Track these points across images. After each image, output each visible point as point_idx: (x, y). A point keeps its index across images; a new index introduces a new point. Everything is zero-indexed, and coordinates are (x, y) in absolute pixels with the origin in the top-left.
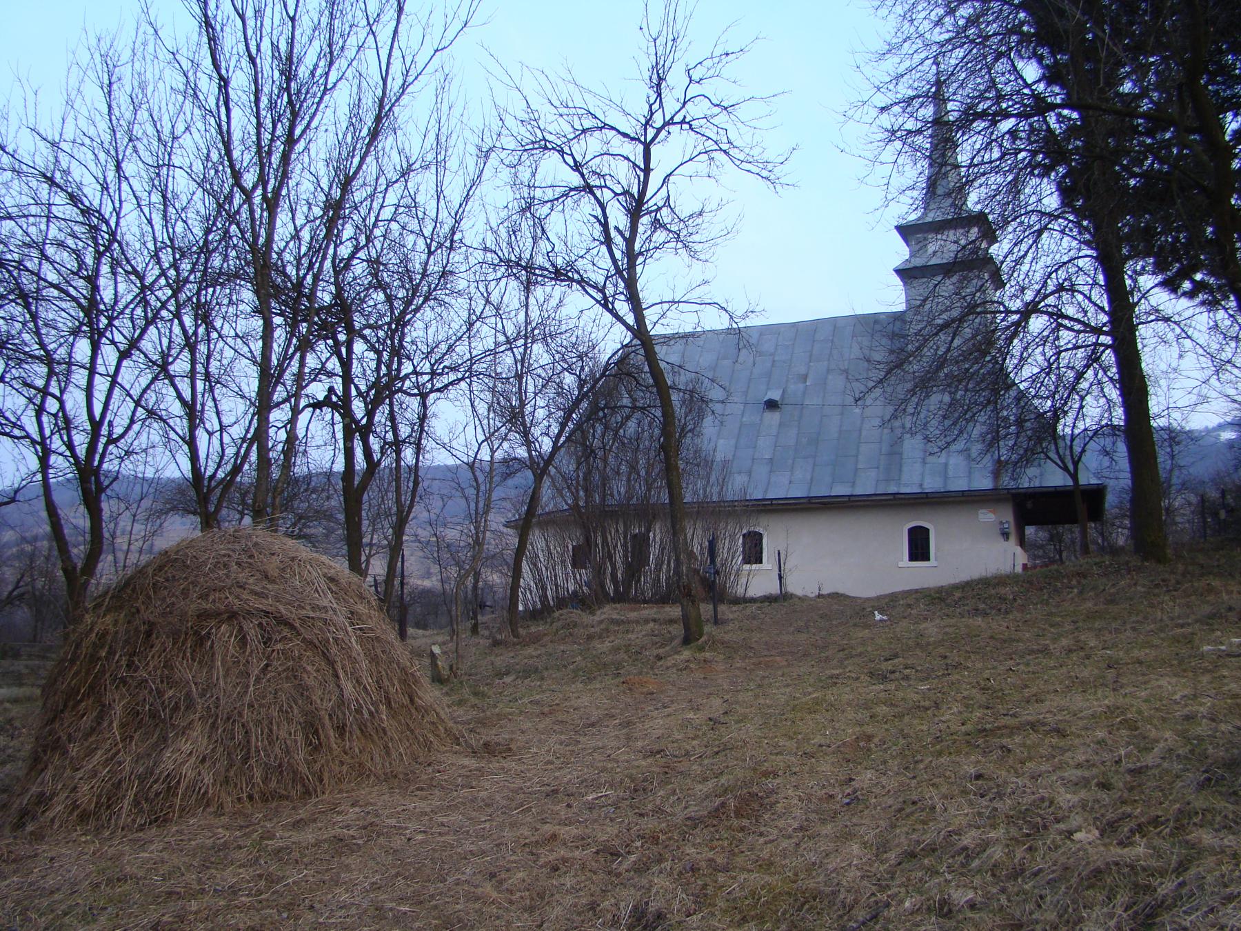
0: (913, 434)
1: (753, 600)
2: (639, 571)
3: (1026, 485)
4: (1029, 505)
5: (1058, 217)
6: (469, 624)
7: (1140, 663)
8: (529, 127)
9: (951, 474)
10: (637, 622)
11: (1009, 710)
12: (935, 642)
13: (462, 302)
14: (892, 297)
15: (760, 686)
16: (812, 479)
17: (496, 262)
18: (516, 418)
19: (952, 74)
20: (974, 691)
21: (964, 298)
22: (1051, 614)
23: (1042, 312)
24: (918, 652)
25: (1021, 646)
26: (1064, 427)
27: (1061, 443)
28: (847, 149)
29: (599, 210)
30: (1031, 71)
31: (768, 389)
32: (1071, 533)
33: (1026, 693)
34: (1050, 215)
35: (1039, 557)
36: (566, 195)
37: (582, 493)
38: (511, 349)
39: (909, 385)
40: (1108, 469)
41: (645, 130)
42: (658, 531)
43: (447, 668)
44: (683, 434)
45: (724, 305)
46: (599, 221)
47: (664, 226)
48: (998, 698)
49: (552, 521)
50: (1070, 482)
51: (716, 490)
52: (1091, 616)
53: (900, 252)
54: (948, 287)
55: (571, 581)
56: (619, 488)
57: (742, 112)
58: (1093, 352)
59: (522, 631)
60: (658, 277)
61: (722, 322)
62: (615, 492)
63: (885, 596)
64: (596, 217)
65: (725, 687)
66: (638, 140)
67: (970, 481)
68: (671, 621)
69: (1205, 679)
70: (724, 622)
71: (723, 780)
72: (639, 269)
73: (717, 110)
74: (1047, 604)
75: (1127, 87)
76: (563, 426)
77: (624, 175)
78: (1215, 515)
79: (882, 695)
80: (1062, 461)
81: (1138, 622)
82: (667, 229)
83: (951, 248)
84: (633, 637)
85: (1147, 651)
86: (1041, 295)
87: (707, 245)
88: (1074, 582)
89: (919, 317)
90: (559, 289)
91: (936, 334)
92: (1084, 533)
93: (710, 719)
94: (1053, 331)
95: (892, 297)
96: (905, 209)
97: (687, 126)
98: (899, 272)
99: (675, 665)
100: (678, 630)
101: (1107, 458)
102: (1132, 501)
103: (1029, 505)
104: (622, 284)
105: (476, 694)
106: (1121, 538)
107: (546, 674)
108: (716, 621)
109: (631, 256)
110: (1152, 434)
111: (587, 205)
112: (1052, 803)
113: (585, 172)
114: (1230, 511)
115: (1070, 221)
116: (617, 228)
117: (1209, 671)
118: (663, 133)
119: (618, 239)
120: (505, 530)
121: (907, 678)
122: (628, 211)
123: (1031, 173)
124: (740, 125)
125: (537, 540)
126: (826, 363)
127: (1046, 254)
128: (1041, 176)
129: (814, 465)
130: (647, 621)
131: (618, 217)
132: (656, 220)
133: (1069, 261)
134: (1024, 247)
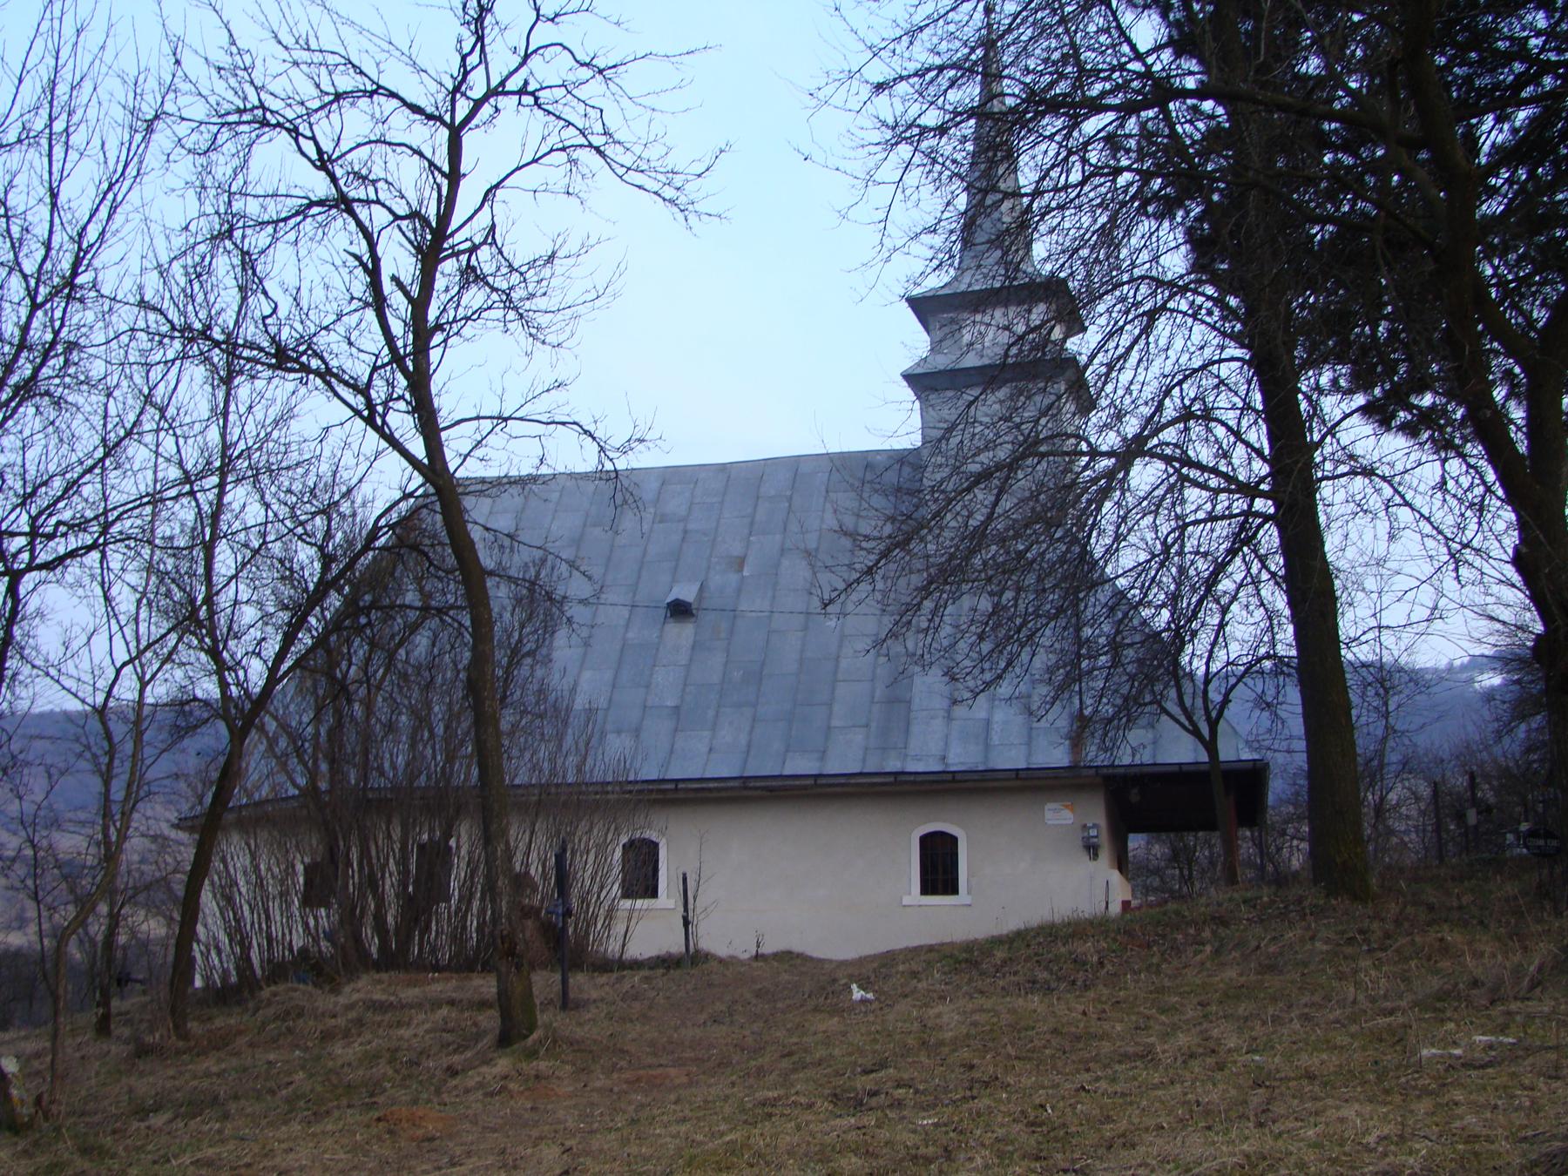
0: (926, 667)
1: (636, 965)
3: (1127, 760)
4: (1134, 795)
5: (1184, 290)
6: (91, 1016)
7: (1311, 1077)
8: (233, 81)
9: (995, 739)
10: (419, 1006)
11: (1074, 1161)
12: (954, 1041)
13: (88, 402)
14: (897, 424)
15: (634, 1122)
16: (749, 746)
17: (165, 329)
18: (197, 620)
19: (1009, 30)
20: (1017, 1127)
21: (1018, 426)
22: (1161, 990)
23: (1153, 456)
25: (1106, 1047)
26: (1194, 658)
27: (1187, 687)
28: (818, 155)
29: (364, 243)
30: (1146, 30)
31: (674, 581)
32: (1205, 846)
33: (1108, 1131)
34: (1171, 284)
35: (1155, 890)
36: (302, 212)
37: (324, 767)
38: (192, 493)
39: (917, 580)
41: (453, 102)
43: (31, 1100)
44: (516, 655)
45: (591, 428)
46: (364, 265)
47: (481, 279)
48: (1056, 1140)
49: (259, 819)
50: (1204, 757)
51: (572, 760)
52: (1234, 994)
53: (912, 342)
54: (992, 404)
55: (296, 930)
56: (395, 756)
57: (629, 80)
58: (1242, 527)
59: (194, 1026)
60: (468, 372)
61: (583, 459)
62: (387, 765)
63: (873, 958)
64: (358, 258)
65: (570, 1124)
66: (440, 119)
67: (1029, 755)
68: (483, 1005)
69: (1423, 1107)
70: (579, 1005)
72: (434, 355)
73: (585, 73)
74: (1158, 973)
75: (1312, 65)
76: (289, 640)
77: (410, 182)
78: (1460, 817)
79: (852, 1136)
80: (1189, 718)
82: (487, 284)
83: (1003, 335)
84: (405, 1032)
85: (1324, 1056)
86: (1152, 425)
87: (559, 316)
88: (1207, 934)
89: (940, 460)
90: (283, 387)
91: (968, 490)
92: (1230, 847)
94: (1170, 489)
95: (897, 424)
96: (919, 266)
97: (530, 100)
99: (481, 1085)
100: (490, 1020)
101: (1266, 714)
102: (1311, 789)
103: (1134, 795)
104: (402, 382)
105: (85, 1151)
106: (1296, 857)
107: (233, 1107)
108: (566, 1002)
109: (422, 331)
110: (1343, 672)
111: (342, 235)
113: (339, 172)
114: (1485, 810)
115: (1209, 298)
117: (1431, 1093)
118: (486, 110)
119: (397, 301)
120: (173, 834)
121: (898, 1104)
122: (419, 249)
123: (1142, 211)
124: (625, 102)
125: (235, 854)
126: (778, 537)
127: (1164, 355)
128: (1159, 217)
130: (436, 1004)
131: (399, 260)
133: (1203, 367)
134: (1125, 340)
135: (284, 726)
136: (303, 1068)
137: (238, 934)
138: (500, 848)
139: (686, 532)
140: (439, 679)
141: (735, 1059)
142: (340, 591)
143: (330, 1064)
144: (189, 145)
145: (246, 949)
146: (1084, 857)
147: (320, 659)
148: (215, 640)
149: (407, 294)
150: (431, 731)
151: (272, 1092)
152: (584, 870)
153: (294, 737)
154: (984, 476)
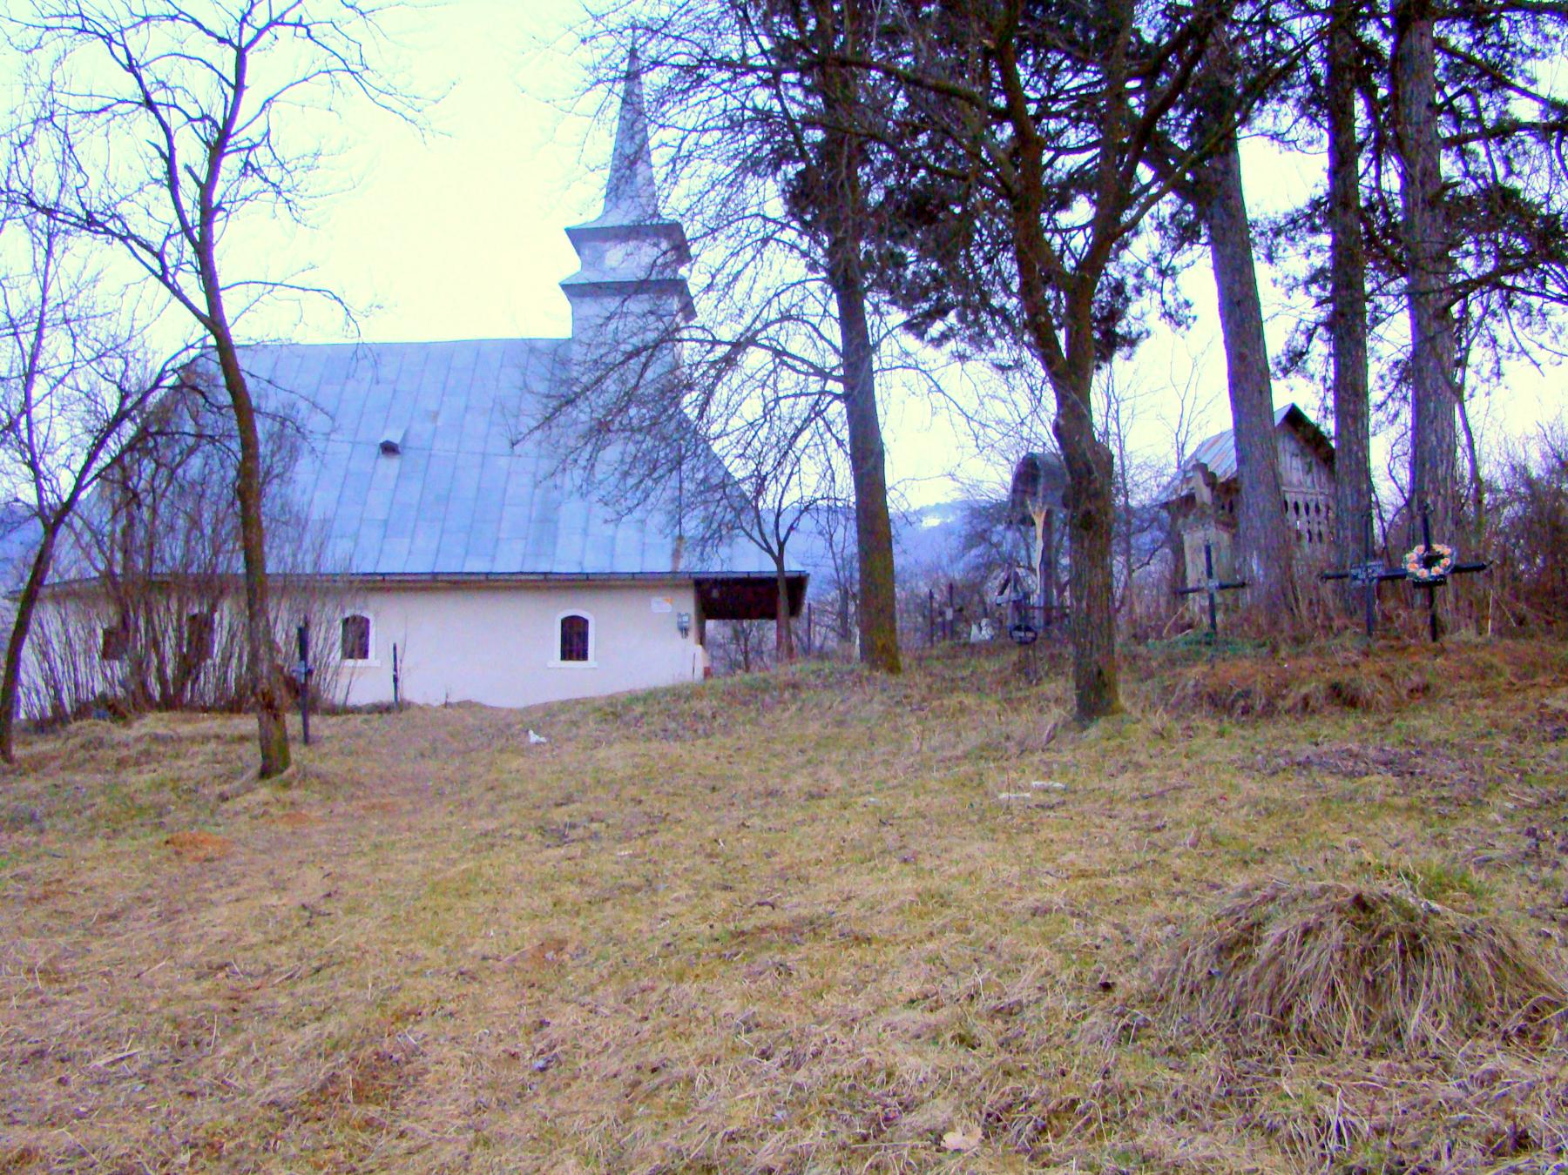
2: (197, 666)
4: (715, 594)
9: (618, 550)
10: (193, 740)
14: (555, 320)
20: (698, 859)
24: (600, 792)
31: (385, 427)
32: (767, 631)
37: (119, 556)
40: (818, 556)
41: (241, 29)
42: (226, 612)
46: (163, 155)
49: (68, 593)
51: (310, 558)
53: (570, 264)
55: (99, 677)
56: (173, 551)
62: (167, 556)
64: (157, 147)
66: (230, 42)
71: (331, 1025)
76: (92, 457)
81: (889, 753)
83: (639, 265)
93: (304, 907)
95: (555, 320)
98: (568, 288)
100: (252, 754)
103: (715, 594)
108: (307, 739)
112: (890, 1075)
116: (189, 169)
118: (267, 36)
120: (1040, 494)
121: (595, 836)
122: (208, 143)
125: (49, 618)
127: (760, 274)
129: (443, 531)
130: (206, 739)
131: (191, 152)
132: (247, 163)
135: (88, 525)
136: (103, 792)
137: (53, 683)
138: (262, 624)
139: (395, 391)
140: (209, 492)
141: (448, 789)
142: (133, 420)
143: (125, 790)
144: (17, 42)
145: (58, 692)
146: (678, 634)
147: (117, 474)
148: (33, 455)
149: (196, 179)
150: (202, 532)
151: (80, 813)
152: (317, 637)
153: (97, 534)
154: (637, 352)
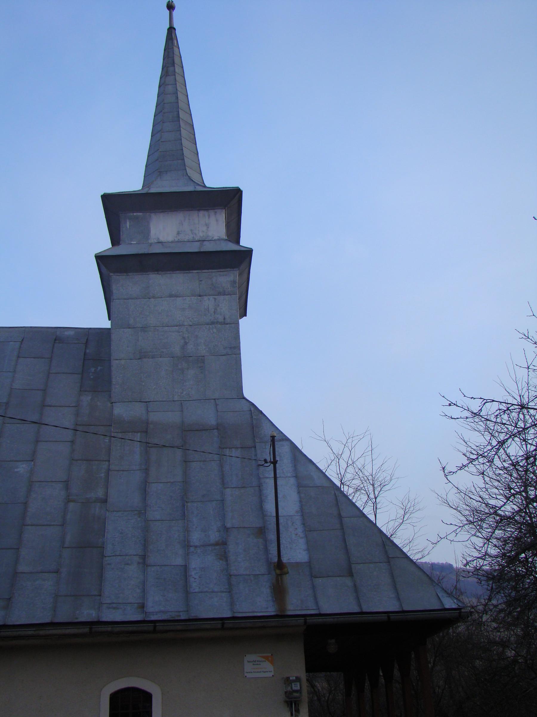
9: (195, 586)
